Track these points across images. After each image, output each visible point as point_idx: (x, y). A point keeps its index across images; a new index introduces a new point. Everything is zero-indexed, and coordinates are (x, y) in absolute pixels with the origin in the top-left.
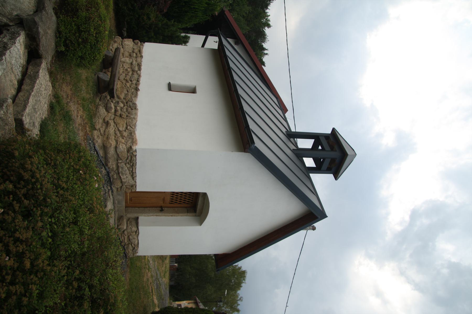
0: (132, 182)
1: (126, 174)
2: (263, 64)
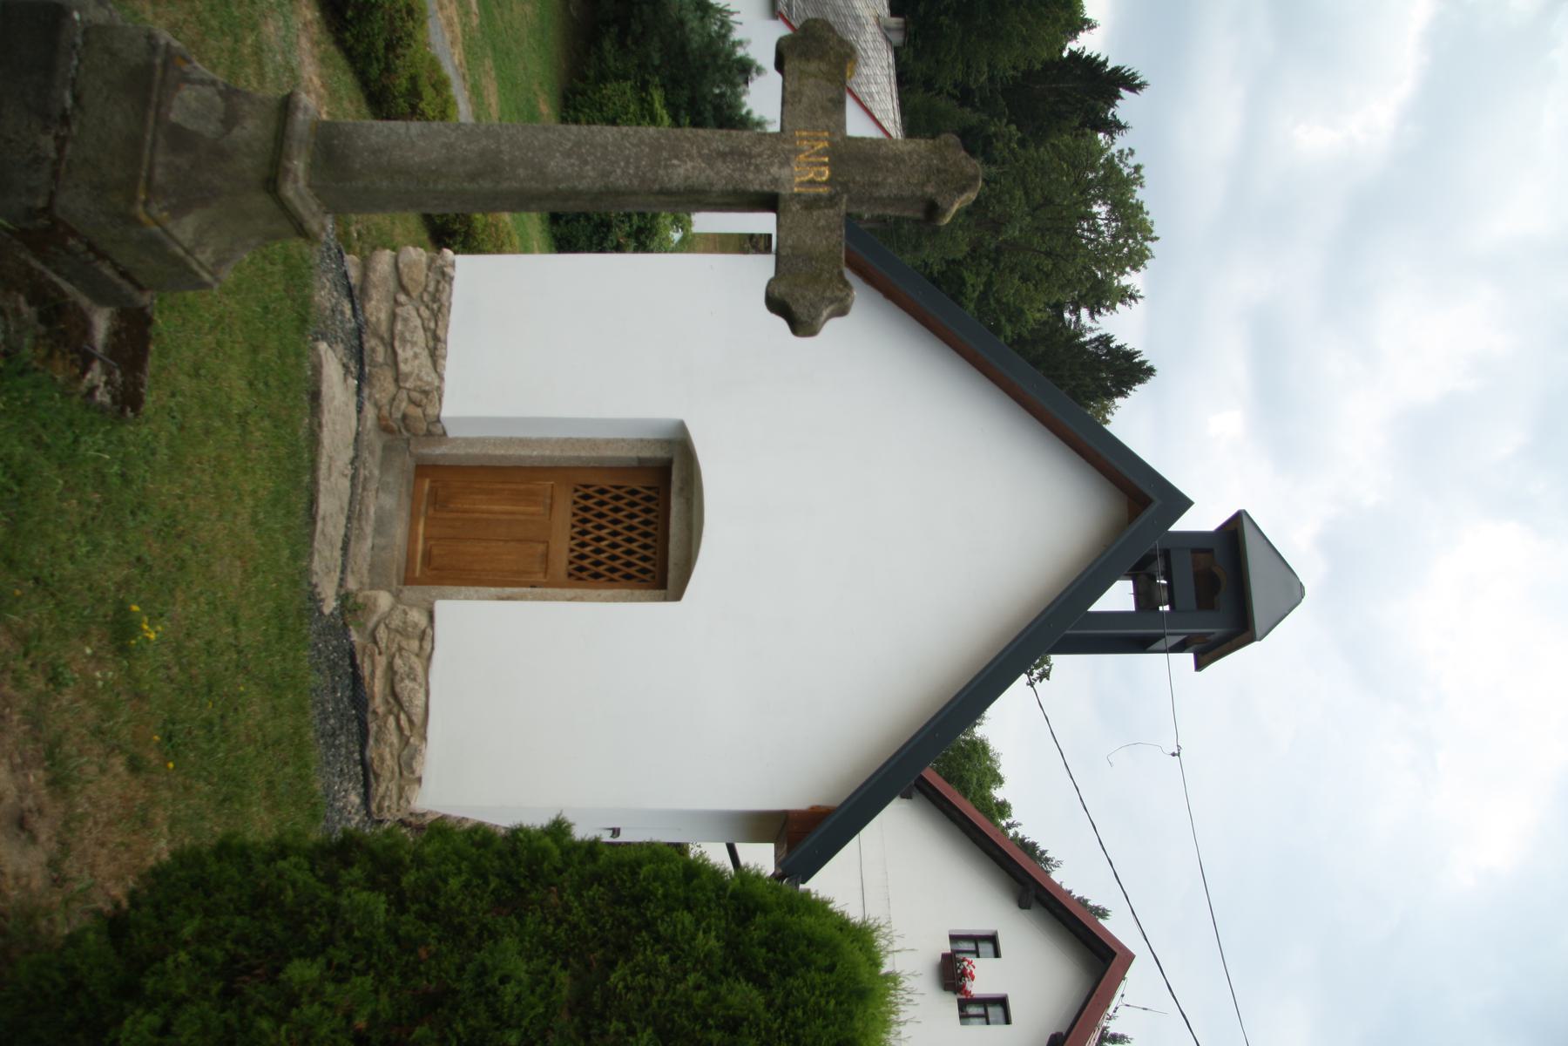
0: (429, 376)
1: (414, 344)
2: (1003, 808)
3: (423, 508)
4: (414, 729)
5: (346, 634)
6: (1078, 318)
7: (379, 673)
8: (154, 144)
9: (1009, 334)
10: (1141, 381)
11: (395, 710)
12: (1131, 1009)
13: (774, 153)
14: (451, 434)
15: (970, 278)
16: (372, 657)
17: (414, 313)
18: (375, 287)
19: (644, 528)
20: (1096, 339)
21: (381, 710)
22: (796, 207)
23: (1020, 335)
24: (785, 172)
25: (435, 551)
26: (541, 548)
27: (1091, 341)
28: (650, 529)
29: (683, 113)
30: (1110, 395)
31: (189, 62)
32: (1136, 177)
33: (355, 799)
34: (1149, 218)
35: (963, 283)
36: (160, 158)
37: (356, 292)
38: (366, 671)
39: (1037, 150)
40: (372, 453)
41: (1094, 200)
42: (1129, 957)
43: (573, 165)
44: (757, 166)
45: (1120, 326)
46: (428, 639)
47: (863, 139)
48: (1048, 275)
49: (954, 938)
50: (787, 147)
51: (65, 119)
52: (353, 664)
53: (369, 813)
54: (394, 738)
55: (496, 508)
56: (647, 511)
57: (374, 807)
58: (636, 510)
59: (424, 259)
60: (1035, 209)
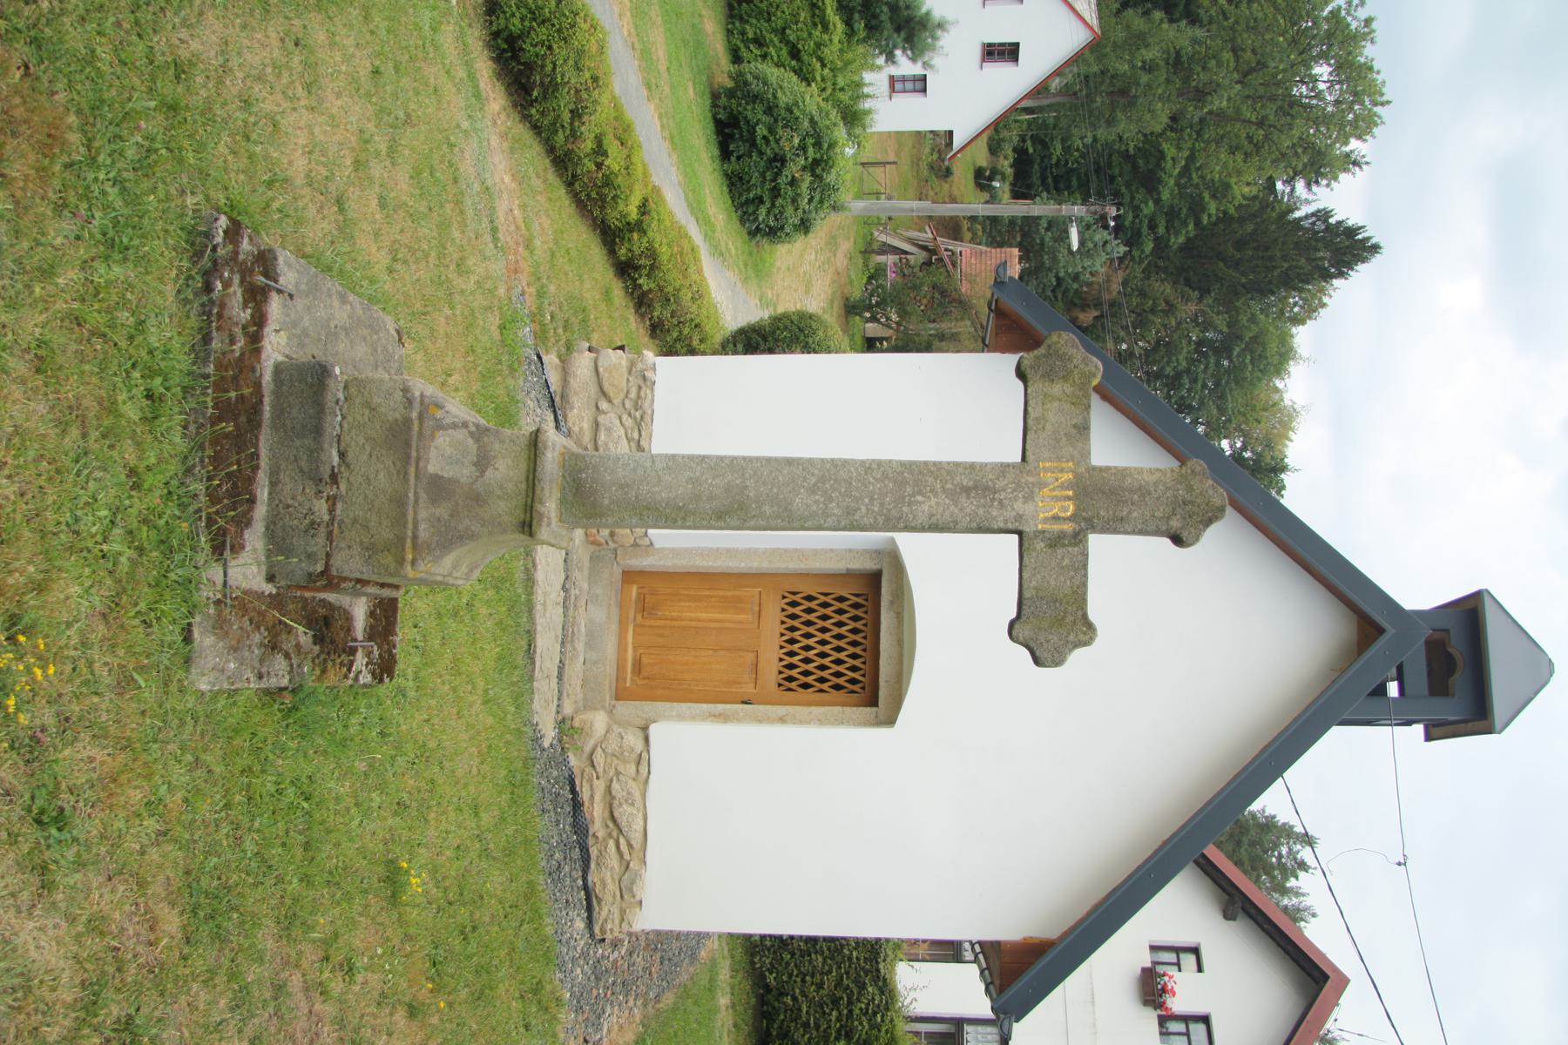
3: (631, 616)
4: (633, 854)
5: (566, 761)
6: (1293, 190)
7: (597, 798)
8: (416, 501)
9: (1213, 211)
10: (1364, 260)
11: (615, 834)
12: (1348, 1017)
13: (1019, 486)
14: (657, 546)
15: (1169, 150)
16: (590, 781)
17: (617, 422)
18: (576, 393)
19: (852, 637)
20: (1313, 214)
21: (601, 834)
22: (1040, 545)
23: (1225, 213)
24: (1030, 507)
25: (645, 660)
26: (750, 657)
27: (1307, 217)
28: (858, 638)
29: (857, 16)
30: (1327, 277)
31: (441, 407)
32: (1367, 30)
33: (580, 925)
34: (1380, 78)
35: (1161, 155)
36: (423, 514)
37: (557, 399)
38: (585, 795)
39: (1249, 7)
40: (580, 569)
41: (1316, 59)
42: (1344, 982)
43: (816, 502)
44: (1000, 501)
45: (1340, 199)
46: (644, 763)
47: (1108, 469)
48: (1258, 147)
49: (1154, 949)
50: (1031, 479)
51: (334, 478)
52: (573, 790)
53: (592, 936)
54: (613, 860)
55: (704, 616)
56: (855, 618)
57: (597, 930)
58: (844, 618)
59: (624, 363)
60: (1246, 75)
